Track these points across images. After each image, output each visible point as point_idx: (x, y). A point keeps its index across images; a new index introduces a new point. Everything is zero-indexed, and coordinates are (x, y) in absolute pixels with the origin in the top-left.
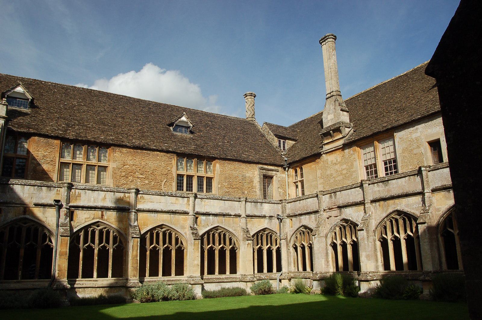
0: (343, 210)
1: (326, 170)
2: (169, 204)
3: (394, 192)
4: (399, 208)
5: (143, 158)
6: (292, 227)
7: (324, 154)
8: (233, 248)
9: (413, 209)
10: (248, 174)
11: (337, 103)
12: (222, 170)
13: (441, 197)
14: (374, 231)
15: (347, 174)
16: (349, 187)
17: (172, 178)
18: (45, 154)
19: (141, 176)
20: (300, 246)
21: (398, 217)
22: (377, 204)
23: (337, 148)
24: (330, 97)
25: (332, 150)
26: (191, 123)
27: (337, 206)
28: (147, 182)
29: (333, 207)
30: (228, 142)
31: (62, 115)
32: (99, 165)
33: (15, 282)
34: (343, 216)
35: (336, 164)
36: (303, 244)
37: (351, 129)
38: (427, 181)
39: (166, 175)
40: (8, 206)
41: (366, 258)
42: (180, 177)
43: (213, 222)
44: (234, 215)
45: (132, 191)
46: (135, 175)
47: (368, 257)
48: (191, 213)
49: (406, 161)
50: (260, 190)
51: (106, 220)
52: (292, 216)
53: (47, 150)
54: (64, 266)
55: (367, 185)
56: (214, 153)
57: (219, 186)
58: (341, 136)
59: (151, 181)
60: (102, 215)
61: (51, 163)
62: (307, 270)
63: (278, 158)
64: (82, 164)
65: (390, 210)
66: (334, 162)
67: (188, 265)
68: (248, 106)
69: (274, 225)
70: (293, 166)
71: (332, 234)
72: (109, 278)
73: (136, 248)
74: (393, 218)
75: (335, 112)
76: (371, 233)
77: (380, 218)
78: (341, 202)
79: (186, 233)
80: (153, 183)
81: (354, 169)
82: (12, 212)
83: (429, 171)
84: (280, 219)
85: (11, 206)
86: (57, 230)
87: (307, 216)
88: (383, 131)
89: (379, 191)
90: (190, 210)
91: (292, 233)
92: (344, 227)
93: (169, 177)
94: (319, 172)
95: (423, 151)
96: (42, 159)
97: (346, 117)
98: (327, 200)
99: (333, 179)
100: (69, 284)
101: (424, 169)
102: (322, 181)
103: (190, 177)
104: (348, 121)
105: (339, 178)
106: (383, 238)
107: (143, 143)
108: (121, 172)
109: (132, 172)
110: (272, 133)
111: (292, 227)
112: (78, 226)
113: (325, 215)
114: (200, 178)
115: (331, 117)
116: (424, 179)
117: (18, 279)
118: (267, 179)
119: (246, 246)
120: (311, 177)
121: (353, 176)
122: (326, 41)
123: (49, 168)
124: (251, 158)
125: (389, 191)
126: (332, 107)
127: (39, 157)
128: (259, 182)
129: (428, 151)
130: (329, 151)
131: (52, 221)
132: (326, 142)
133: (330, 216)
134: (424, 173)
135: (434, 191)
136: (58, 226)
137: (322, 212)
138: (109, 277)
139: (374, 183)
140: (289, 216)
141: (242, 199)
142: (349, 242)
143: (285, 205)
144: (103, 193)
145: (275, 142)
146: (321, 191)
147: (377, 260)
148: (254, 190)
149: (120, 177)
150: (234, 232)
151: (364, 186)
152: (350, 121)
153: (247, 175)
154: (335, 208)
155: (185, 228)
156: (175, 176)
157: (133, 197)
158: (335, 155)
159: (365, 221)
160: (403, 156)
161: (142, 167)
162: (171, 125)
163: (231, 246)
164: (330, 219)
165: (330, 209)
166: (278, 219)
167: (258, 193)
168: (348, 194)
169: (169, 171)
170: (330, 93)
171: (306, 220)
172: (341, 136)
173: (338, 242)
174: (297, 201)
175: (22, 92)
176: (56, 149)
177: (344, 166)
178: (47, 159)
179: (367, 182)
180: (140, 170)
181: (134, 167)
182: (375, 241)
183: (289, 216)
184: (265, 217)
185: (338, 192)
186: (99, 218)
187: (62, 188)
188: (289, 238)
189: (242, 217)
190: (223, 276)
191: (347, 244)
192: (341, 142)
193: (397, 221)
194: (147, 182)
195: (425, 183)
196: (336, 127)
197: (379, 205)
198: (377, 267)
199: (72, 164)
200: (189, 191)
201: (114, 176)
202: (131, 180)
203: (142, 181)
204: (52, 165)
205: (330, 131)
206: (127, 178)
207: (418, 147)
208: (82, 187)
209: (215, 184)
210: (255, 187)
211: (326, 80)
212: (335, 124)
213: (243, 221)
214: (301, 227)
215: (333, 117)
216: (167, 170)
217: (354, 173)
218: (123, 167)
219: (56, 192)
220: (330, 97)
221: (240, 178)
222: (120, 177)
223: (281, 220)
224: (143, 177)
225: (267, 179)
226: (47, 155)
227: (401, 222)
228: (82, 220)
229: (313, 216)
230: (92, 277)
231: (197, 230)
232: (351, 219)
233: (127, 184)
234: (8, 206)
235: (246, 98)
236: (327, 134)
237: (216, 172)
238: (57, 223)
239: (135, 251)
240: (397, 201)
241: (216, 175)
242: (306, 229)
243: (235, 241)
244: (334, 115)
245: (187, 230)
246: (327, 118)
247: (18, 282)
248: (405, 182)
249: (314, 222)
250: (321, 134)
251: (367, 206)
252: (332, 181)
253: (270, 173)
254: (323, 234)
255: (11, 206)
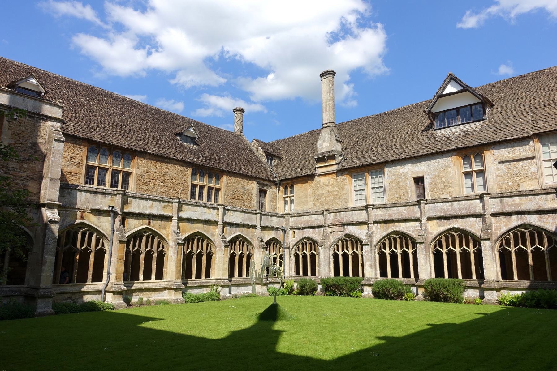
0: (346, 227)
1: (318, 189)
2: (203, 214)
3: (394, 217)
4: (398, 229)
5: (163, 167)
6: (294, 238)
7: (317, 175)
8: (249, 253)
9: (410, 231)
10: (248, 187)
11: (333, 133)
12: (228, 182)
13: (434, 224)
14: (375, 246)
15: (338, 195)
16: (354, 209)
17: (188, 187)
18: (73, 155)
19: (162, 184)
20: (302, 255)
21: (396, 237)
22: (379, 225)
23: (329, 172)
24: (326, 127)
25: (325, 173)
26: (197, 135)
27: (341, 223)
28: (166, 189)
29: (338, 224)
30: (227, 155)
31: (77, 113)
32: (124, 170)
33: (71, 286)
34: (347, 232)
35: (328, 186)
36: (304, 253)
37: (343, 157)
38: (425, 211)
39: (182, 184)
40: (66, 211)
41: (369, 267)
42: (194, 186)
43: (237, 232)
44: (251, 226)
45: (175, 200)
46: (156, 182)
47: (371, 266)
48: (220, 222)
49: (393, 190)
50: (257, 202)
51: (152, 227)
52: (295, 229)
53: (75, 151)
54: (121, 270)
55: (371, 209)
56: (223, 166)
57: (225, 197)
58: (334, 162)
59: (170, 189)
60: (149, 222)
61: (78, 165)
62: (308, 275)
63: (266, 174)
64: (108, 169)
65: (390, 230)
66: (326, 184)
67: (216, 268)
68: (237, 120)
69: (279, 235)
70: (284, 183)
71: (334, 246)
72: (153, 280)
73: (180, 253)
74: (392, 237)
75: (331, 141)
76: (373, 248)
77: (381, 236)
78: (345, 221)
79: (215, 240)
80: (171, 191)
81: (345, 192)
82: (69, 216)
83: (426, 204)
84: (284, 230)
85: (69, 211)
86: (112, 235)
87: (311, 230)
88: (375, 164)
89: (381, 215)
90: (220, 220)
91: (294, 243)
92: (347, 241)
93: (185, 186)
94: (310, 191)
95: (408, 184)
96: (69, 160)
97: (339, 146)
98: (332, 217)
99: (324, 198)
100: (125, 286)
101: (423, 202)
102: (313, 198)
103: (202, 187)
104: (340, 150)
105: (329, 198)
106: (382, 252)
107: (162, 151)
108: (144, 178)
109: (154, 180)
110: (261, 150)
111: (294, 238)
112: (128, 231)
113: (330, 230)
114: (210, 189)
115: (326, 144)
116: (423, 210)
117: (74, 282)
118: (263, 192)
119: (262, 253)
120: (302, 194)
121: (344, 198)
122: (327, 76)
123: (76, 170)
124: (250, 173)
125: (390, 215)
126: (328, 136)
127: (66, 159)
128: (257, 195)
129: (411, 183)
130: (322, 174)
131: (106, 226)
132: (319, 165)
133: (334, 231)
134: (422, 205)
135: (429, 219)
136: (113, 231)
137: (326, 228)
138: (152, 279)
139: (377, 208)
140: (291, 229)
141: (258, 212)
142: (350, 254)
143: (289, 219)
144: (150, 203)
145: (264, 160)
146: (327, 210)
147: (376, 269)
148: (252, 202)
149: (143, 184)
150: (250, 240)
151: (369, 209)
152: (342, 149)
153: (248, 188)
154: (339, 225)
155: (215, 236)
156: (190, 185)
157: (176, 206)
158: (328, 178)
159: (369, 236)
160: (391, 186)
161: (162, 175)
162: (180, 134)
163: (248, 253)
164: (333, 233)
165: (333, 225)
166: (282, 230)
167: (255, 205)
168: (352, 214)
169: (185, 180)
170: (327, 124)
171: (309, 233)
172: (335, 163)
173: (340, 253)
174: (302, 216)
175: (35, 84)
176: (83, 151)
177: (336, 189)
178: (75, 161)
179: (372, 207)
180: (160, 178)
181: (155, 175)
182: (375, 253)
183: (292, 228)
184: (273, 228)
185: (342, 212)
186: (146, 224)
187: (115, 195)
188: (291, 248)
189: (257, 227)
190: (241, 279)
191: (348, 255)
192: (335, 168)
193: (395, 239)
194: (166, 189)
195: (423, 212)
196: (331, 154)
197: (381, 226)
198: (376, 274)
199: (122, 172)
200: (114, 187)
201: (137, 183)
202: (152, 187)
203: (162, 189)
204: (79, 167)
205: (324, 157)
206: (149, 184)
207: (405, 180)
208: (133, 194)
209: (221, 195)
210: (253, 199)
211: (323, 111)
212: (329, 152)
213: (258, 230)
214: (304, 238)
215: (328, 145)
216: (183, 180)
217: (344, 195)
218: (146, 174)
219: (110, 199)
220: (326, 127)
221: (242, 190)
222: (143, 184)
223: (284, 231)
224: (163, 184)
225: (263, 192)
226: (74, 157)
227: (398, 240)
228: (132, 225)
229: (317, 230)
230: (139, 280)
231: (225, 237)
232: (354, 235)
233: (148, 190)
234: (66, 211)
235: (235, 113)
236: (320, 160)
237: (223, 184)
238: (112, 227)
239: (179, 255)
240: (397, 224)
241: (223, 186)
242: (308, 240)
243: (251, 248)
244: (330, 144)
245: (216, 237)
246: (322, 145)
247: (74, 285)
248: (405, 209)
249: (318, 235)
250: (316, 159)
251: (370, 226)
252: (323, 199)
253: (265, 188)
254: (327, 246)
255: (69, 211)
